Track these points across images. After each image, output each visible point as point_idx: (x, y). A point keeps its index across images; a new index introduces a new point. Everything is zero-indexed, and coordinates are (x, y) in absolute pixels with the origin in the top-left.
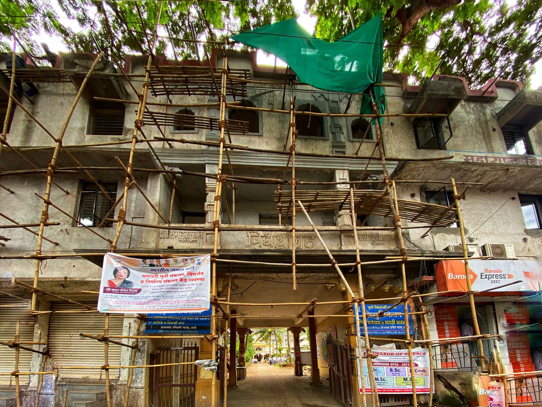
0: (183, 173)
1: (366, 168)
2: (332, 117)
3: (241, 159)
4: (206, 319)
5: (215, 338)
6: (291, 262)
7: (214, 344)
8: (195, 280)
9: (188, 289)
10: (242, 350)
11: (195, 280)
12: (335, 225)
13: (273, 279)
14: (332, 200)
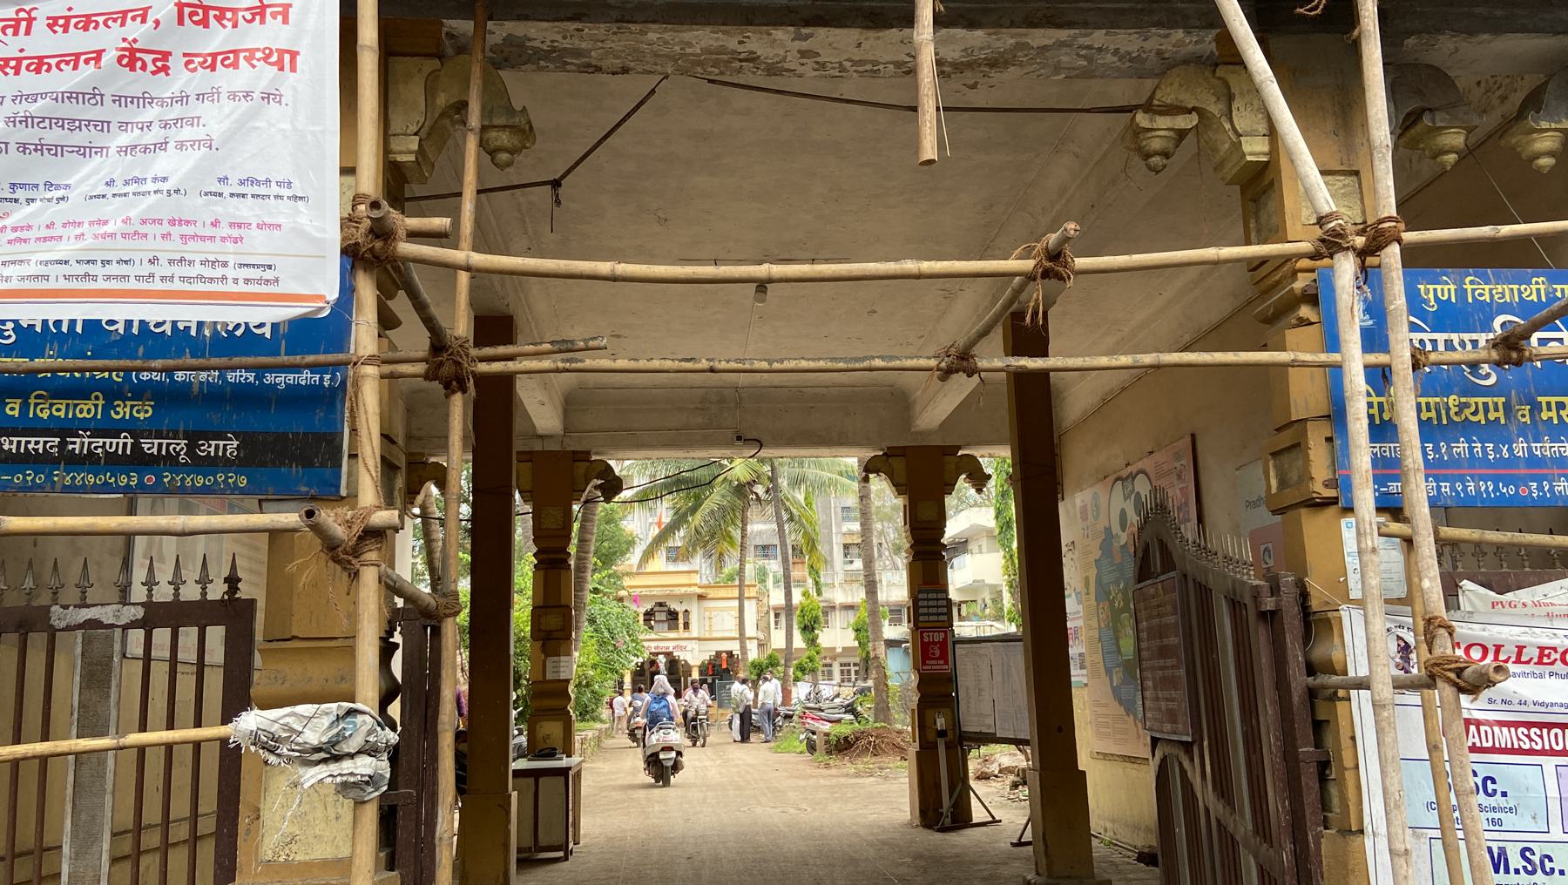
4: (306, 378)
7: (369, 576)
10: (553, 621)
11: (230, 58)
13: (773, 70)
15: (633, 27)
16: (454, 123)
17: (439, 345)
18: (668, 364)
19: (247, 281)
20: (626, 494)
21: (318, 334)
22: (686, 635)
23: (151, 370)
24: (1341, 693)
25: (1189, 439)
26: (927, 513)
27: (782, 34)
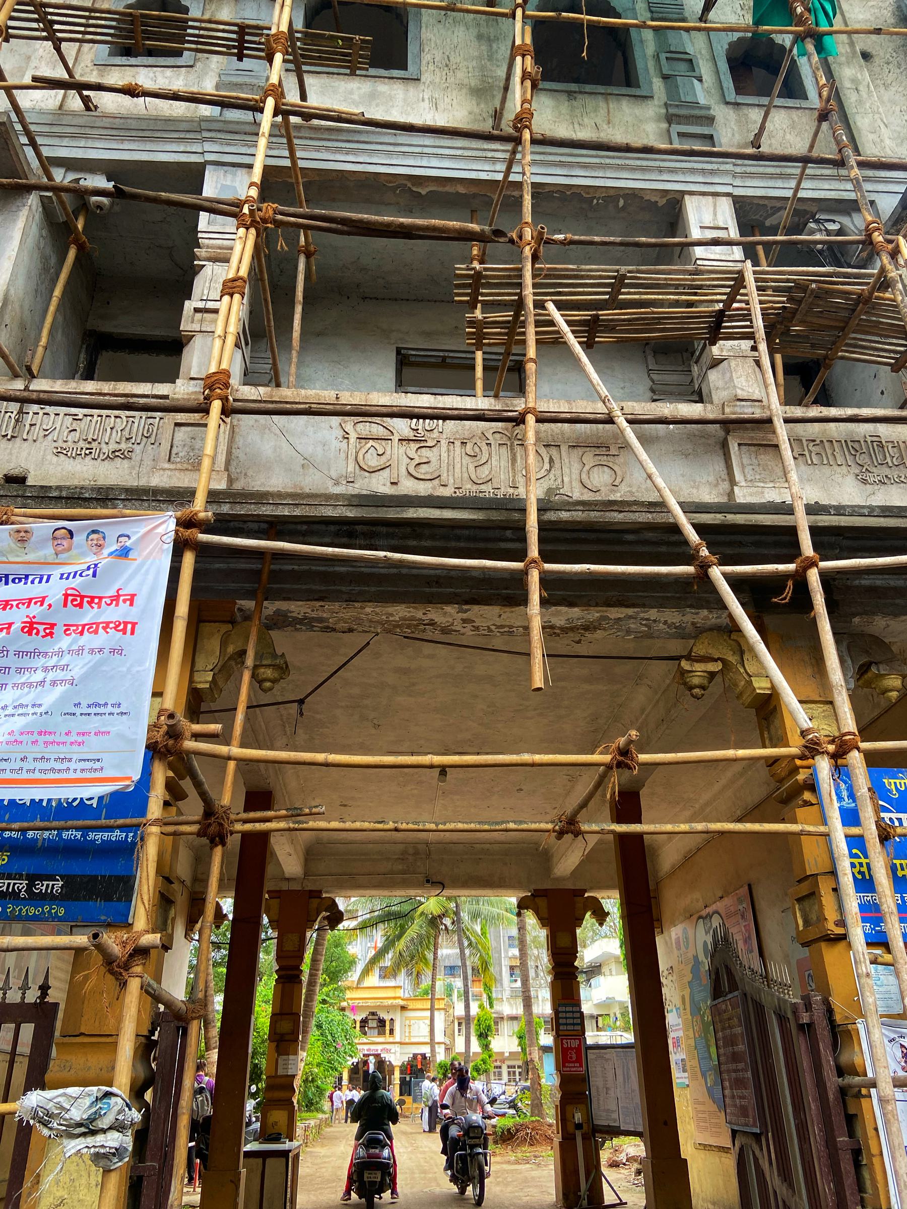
0: (117, 194)
1: (796, 190)
2: (655, 29)
3: (338, 150)
4: (117, 835)
5: (142, 952)
6: (520, 554)
7: (134, 985)
8: (93, 628)
9: (51, 676)
10: (285, 1026)
11: (93, 628)
12: (701, 400)
13: (445, 631)
14: (677, 304)
15: (356, 604)
16: (237, 663)
17: (209, 812)
18: (366, 825)
19: (83, 770)
20: (345, 924)
21: (126, 803)
22: (391, 1040)
23: (11, 830)
24: (864, 1091)
25: (747, 887)
26: (564, 942)
27: (450, 609)
